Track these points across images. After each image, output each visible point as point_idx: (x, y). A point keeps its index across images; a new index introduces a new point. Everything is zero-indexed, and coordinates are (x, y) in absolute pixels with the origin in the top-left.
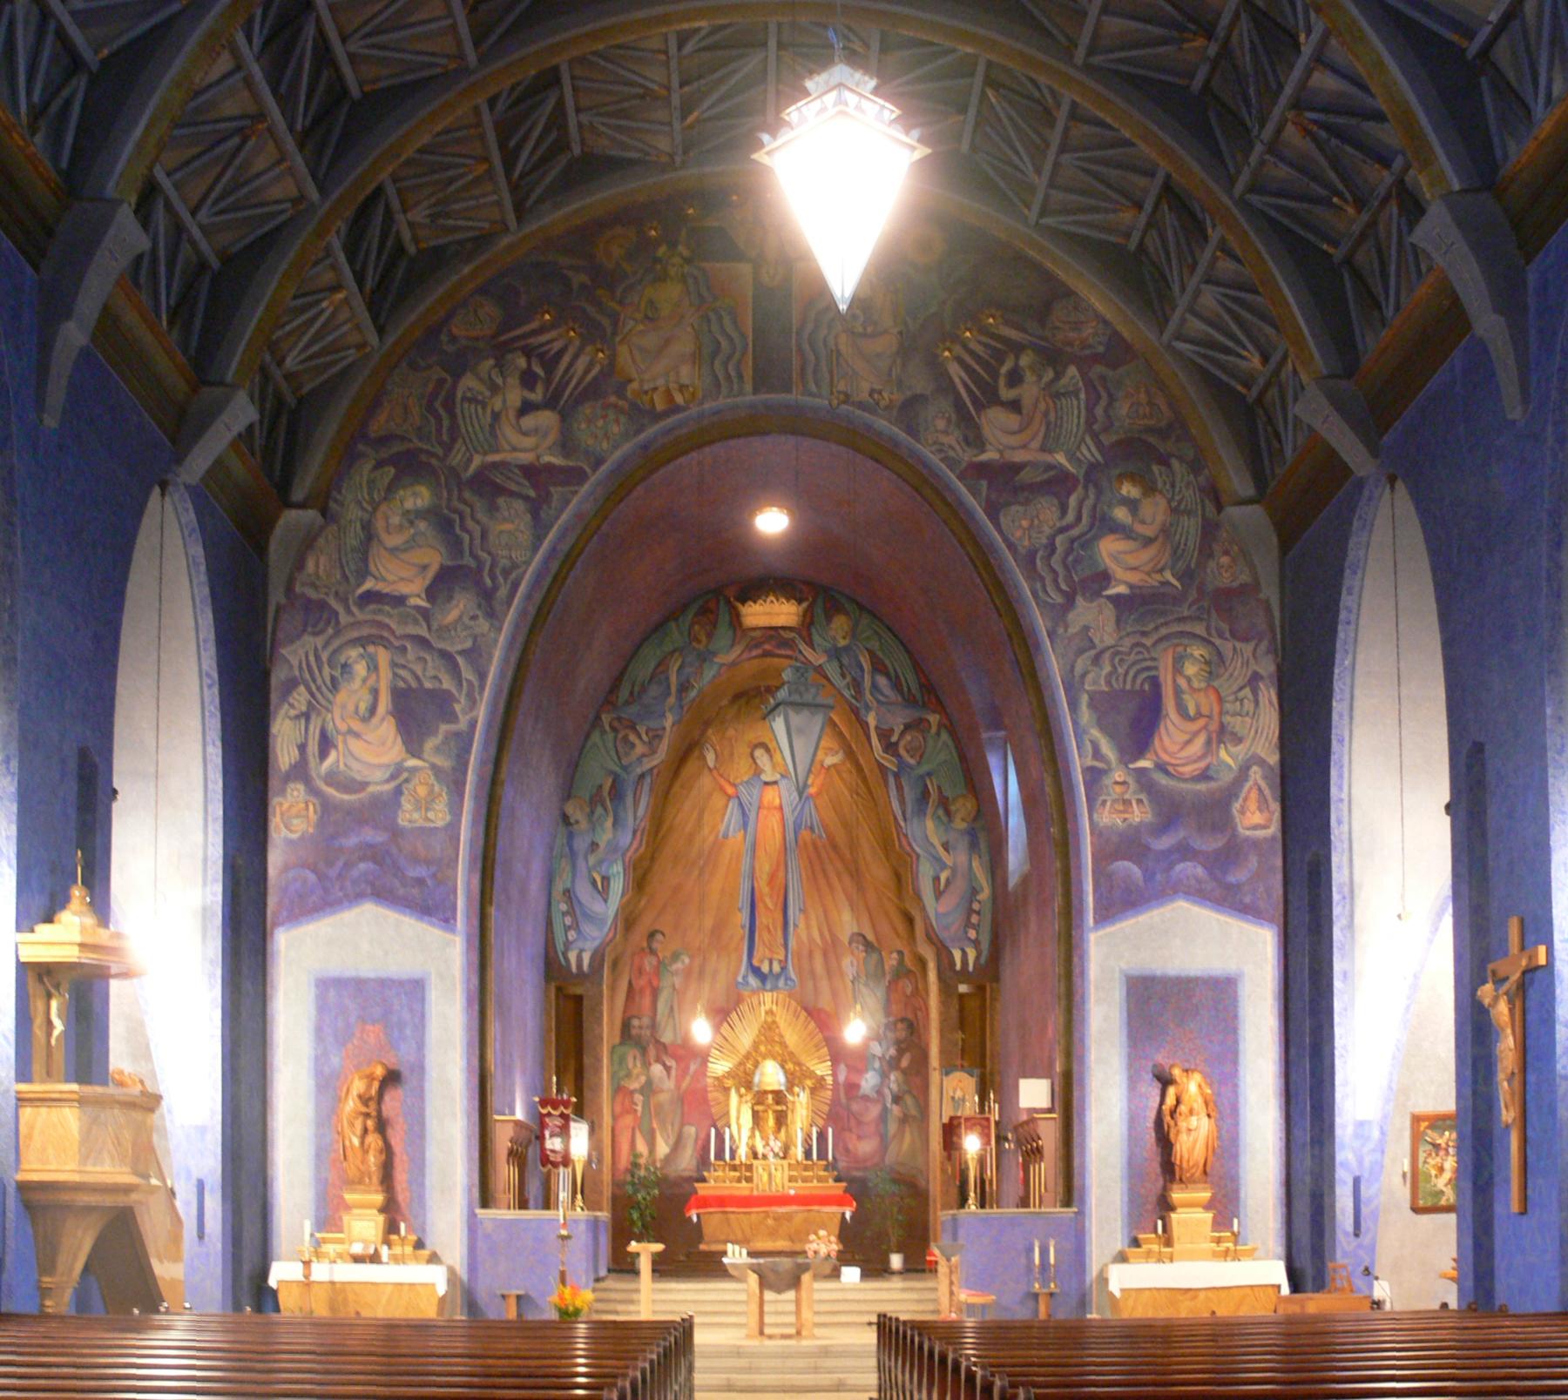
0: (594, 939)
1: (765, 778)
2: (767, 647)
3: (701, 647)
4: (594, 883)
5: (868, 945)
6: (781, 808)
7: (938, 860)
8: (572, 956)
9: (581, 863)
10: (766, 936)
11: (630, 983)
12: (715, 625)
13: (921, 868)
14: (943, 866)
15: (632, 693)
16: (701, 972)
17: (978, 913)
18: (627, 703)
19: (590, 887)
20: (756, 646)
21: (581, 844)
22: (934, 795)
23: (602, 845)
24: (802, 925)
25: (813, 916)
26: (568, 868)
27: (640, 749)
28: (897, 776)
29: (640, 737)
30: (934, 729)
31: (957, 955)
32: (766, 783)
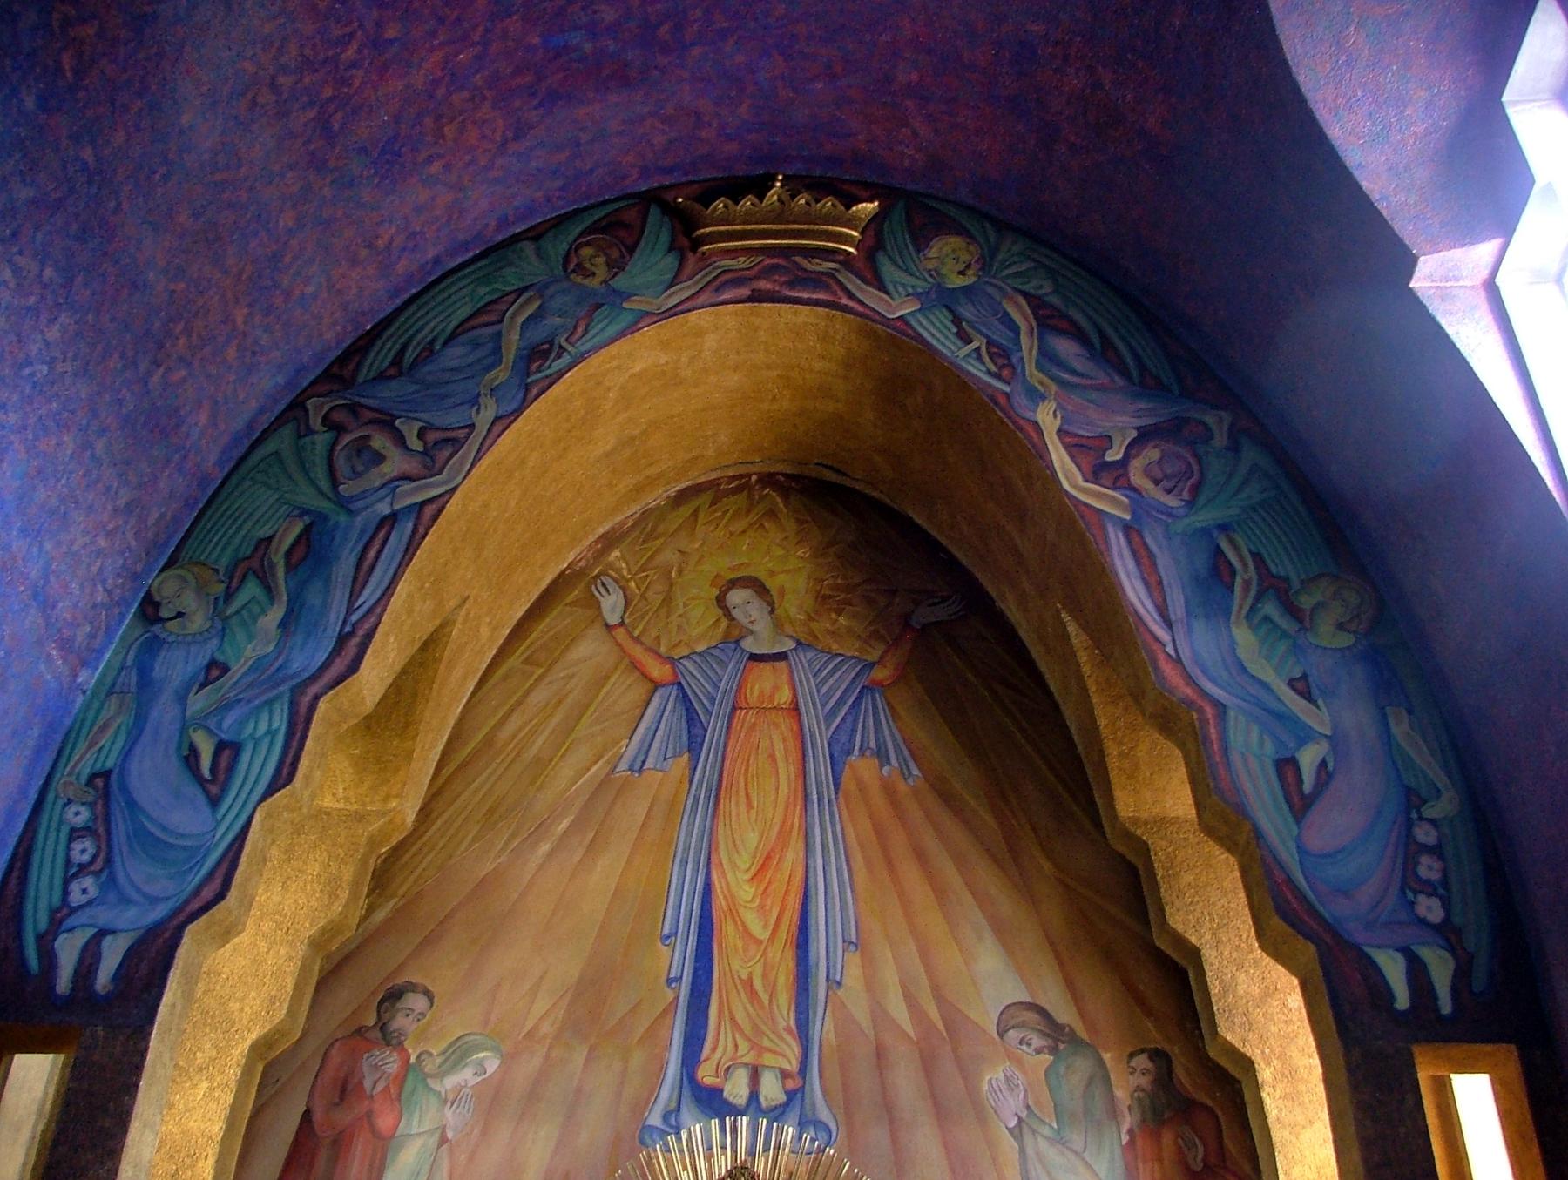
0: (154, 900)
1: (749, 645)
2: (764, 285)
3: (594, 283)
4: (194, 752)
5: (1056, 1033)
6: (795, 708)
7: (1284, 717)
8: (68, 951)
9: (164, 713)
10: (741, 1008)
11: (307, 1116)
12: (631, 250)
13: (1236, 738)
14: (1305, 736)
15: (397, 361)
16: (533, 1095)
17: (1436, 851)
18: (382, 377)
19: (175, 765)
20: (738, 282)
21: (176, 667)
22: (1246, 573)
23: (238, 669)
24: (853, 975)
25: (885, 955)
26: (125, 720)
27: (396, 463)
28: (1127, 529)
29: (400, 440)
30: (1220, 440)
31: (1393, 970)
32: (754, 657)
